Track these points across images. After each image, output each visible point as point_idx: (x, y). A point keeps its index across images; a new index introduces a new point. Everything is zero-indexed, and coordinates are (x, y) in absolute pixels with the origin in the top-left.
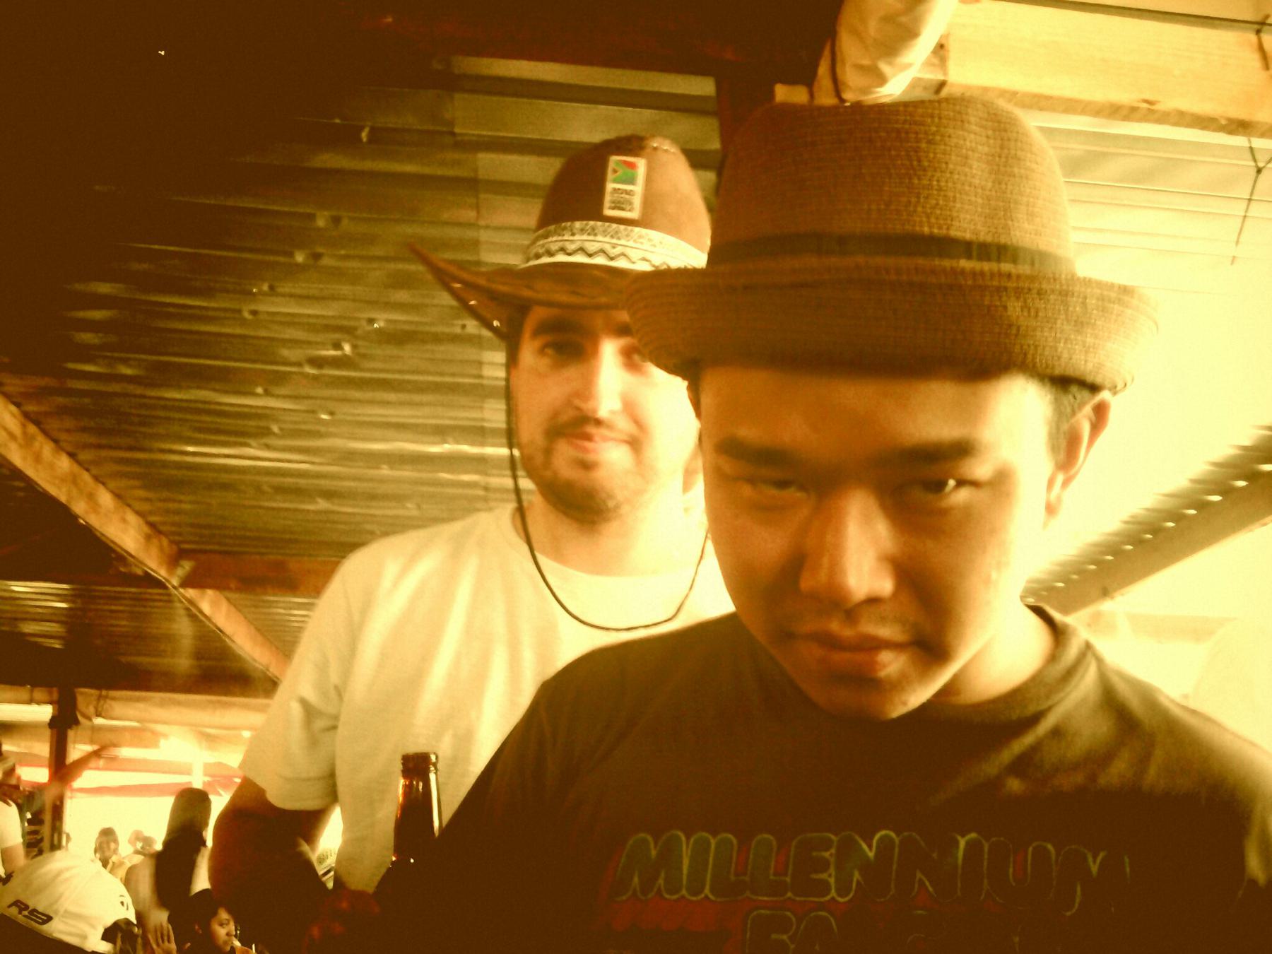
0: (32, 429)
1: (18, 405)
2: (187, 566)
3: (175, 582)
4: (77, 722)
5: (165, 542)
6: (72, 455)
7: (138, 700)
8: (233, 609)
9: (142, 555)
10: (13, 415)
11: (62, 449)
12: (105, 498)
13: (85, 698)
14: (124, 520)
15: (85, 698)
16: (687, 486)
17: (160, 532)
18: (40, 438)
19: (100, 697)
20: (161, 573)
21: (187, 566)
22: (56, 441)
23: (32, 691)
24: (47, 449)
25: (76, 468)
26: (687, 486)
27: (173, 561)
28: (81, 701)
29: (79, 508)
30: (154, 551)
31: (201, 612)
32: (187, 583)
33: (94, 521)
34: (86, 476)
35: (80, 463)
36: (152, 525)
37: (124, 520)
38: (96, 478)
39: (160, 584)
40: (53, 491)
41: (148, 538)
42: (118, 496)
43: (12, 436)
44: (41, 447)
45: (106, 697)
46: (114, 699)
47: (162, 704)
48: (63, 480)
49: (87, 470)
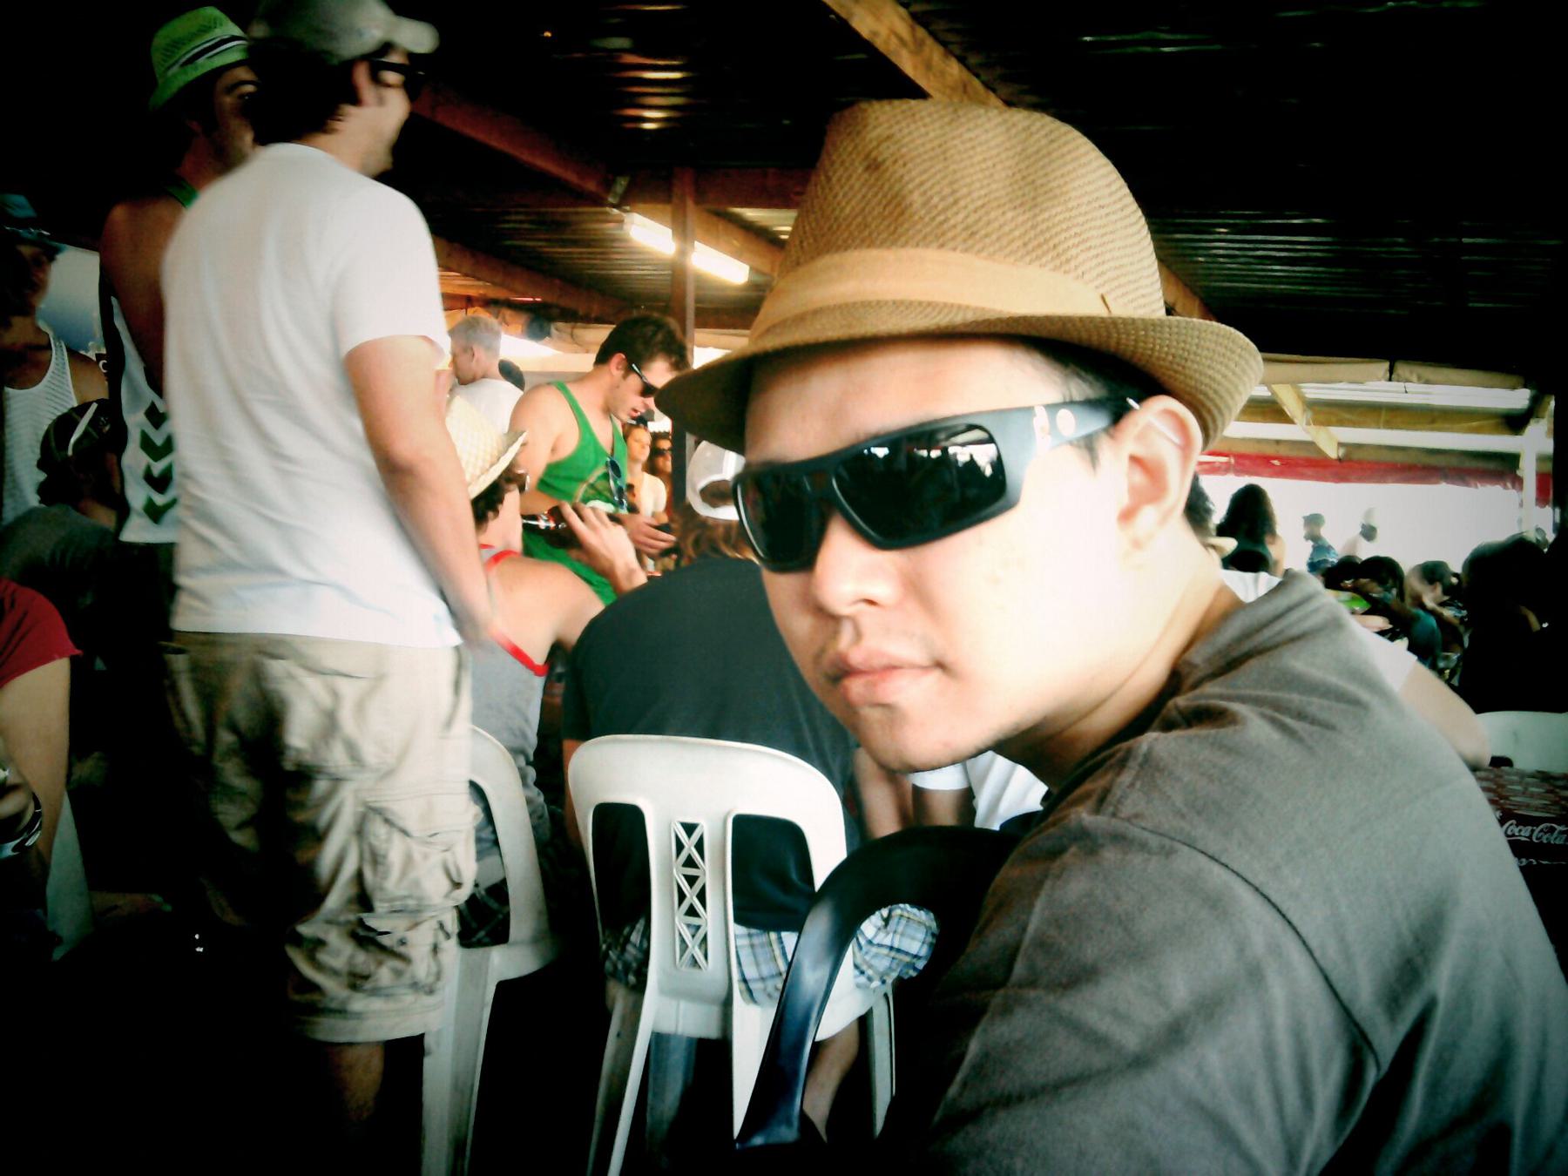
0: (921, 32)
18: (930, 41)
25: (966, 75)
49: (977, 76)
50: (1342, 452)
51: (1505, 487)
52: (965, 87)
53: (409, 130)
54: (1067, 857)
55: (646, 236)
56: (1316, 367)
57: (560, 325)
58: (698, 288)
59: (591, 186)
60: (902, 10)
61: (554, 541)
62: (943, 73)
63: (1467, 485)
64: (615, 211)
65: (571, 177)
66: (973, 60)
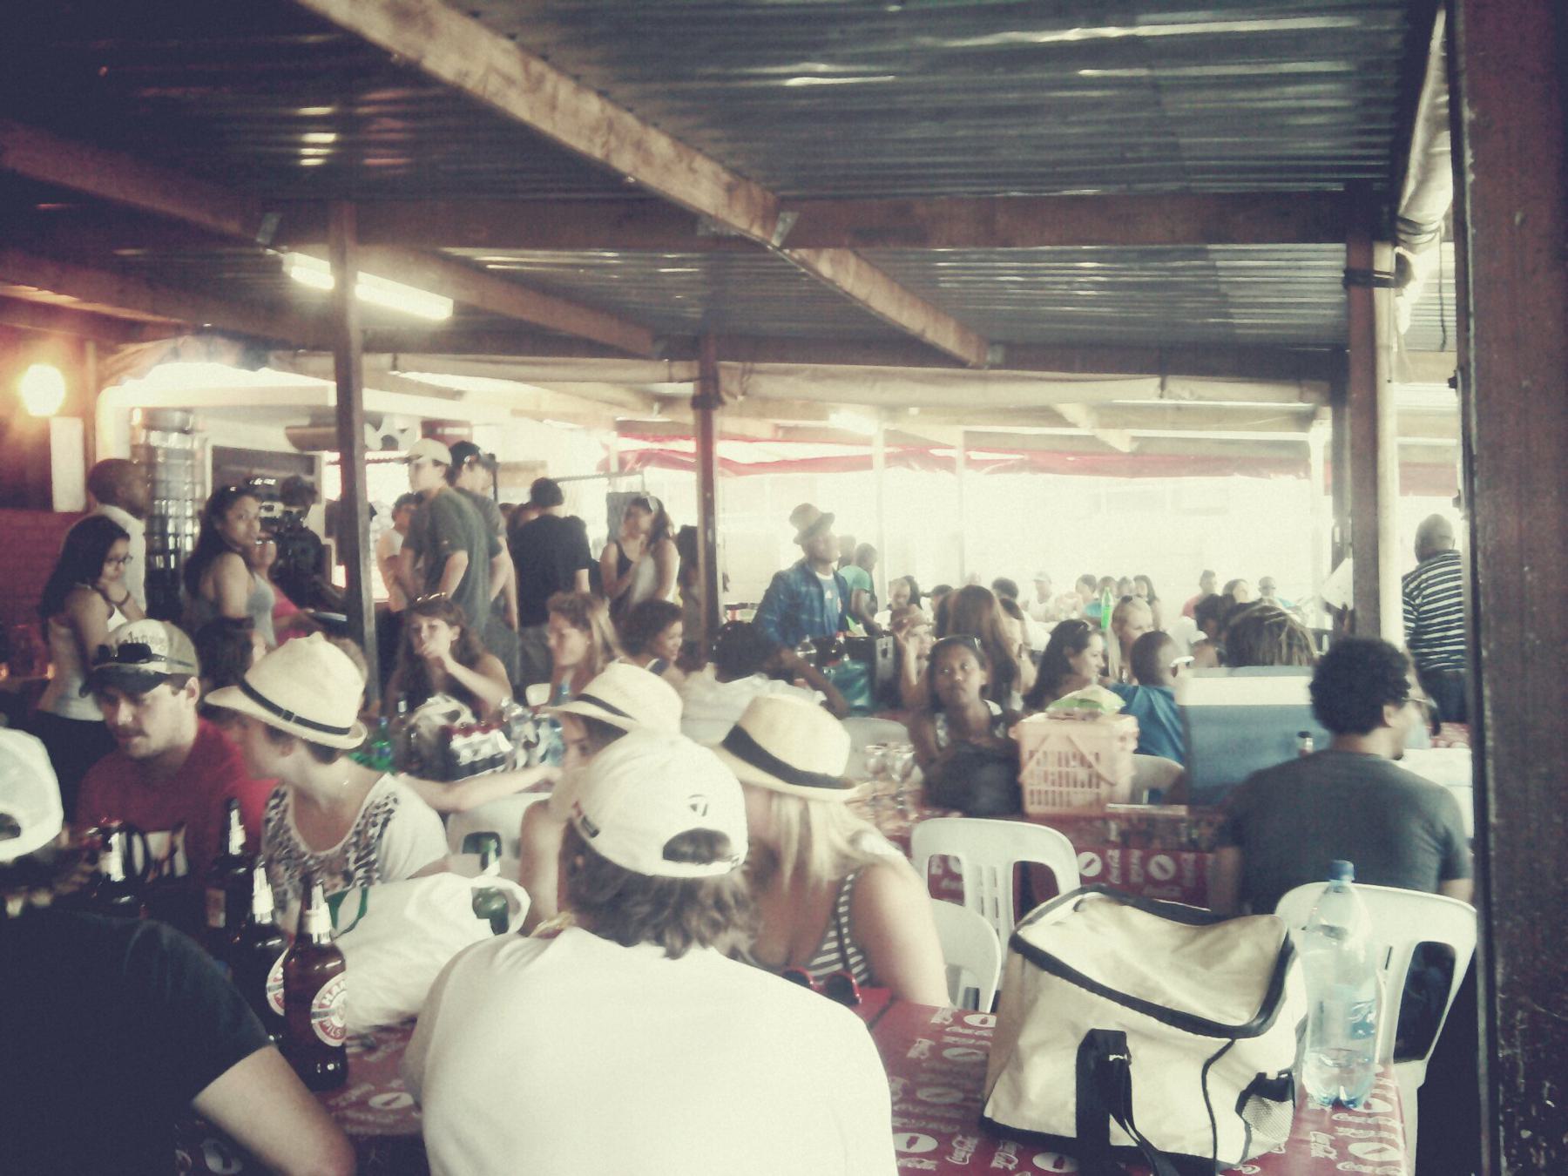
0: (537, 66)
1: (512, 37)
2: (788, 220)
3: (776, 242)
4: (721, 402)
5: (756, 191)
6: (602, 94)
7: (787, 373)
8: (865, 265)
9: (723, 214)
10: (505, 51)
11: (589, 87)
12: (661, 145)
13: (729, 371)
14: (692, 170)
15: (729, 371)
16: (1336, 564)
17: (748, 179)
18: (551, 78)
19: (744, 372)
20: (757, 232)
21: (788, 220)
22: (577, 78)
23: (670, 366)
24: (564, 90)
25: (611, 111)
26: (1336, 564)
27: (769, 217)
28: (724, 378)
29: (624, 162)
30: (739, 208)
31: (821, 276)
32: (791, 241)
33: (649, 177)
34: (629, 120)
35: (616, 102)
36: (734, 171)
37: (692, 170)
38: (643, 120)
39: (757, 246)
40: (581, 145)
41: (730, 189)
42: (677, 138)
43: (509, 81)
44: (555, 88)
45: (751, 371)
46: (760, 372)
47: (814, 378)
48: (595, 129)
49: (630, 110)
50: (1135, 446)
51: (1299, 477)
52: (611, 127)
53: (908, 1048)
54: (1183, 708)
55: (308, 272)
56: (1094, 385)
57: (280, 353)
58: (364, 332)
59: (232, 227)
60: (507, 44)
61: (540, 80)
62: (575, 113)
63: (1259, 475)
64: (270, 252)
65: (207, 219)
66: (623, 91)
